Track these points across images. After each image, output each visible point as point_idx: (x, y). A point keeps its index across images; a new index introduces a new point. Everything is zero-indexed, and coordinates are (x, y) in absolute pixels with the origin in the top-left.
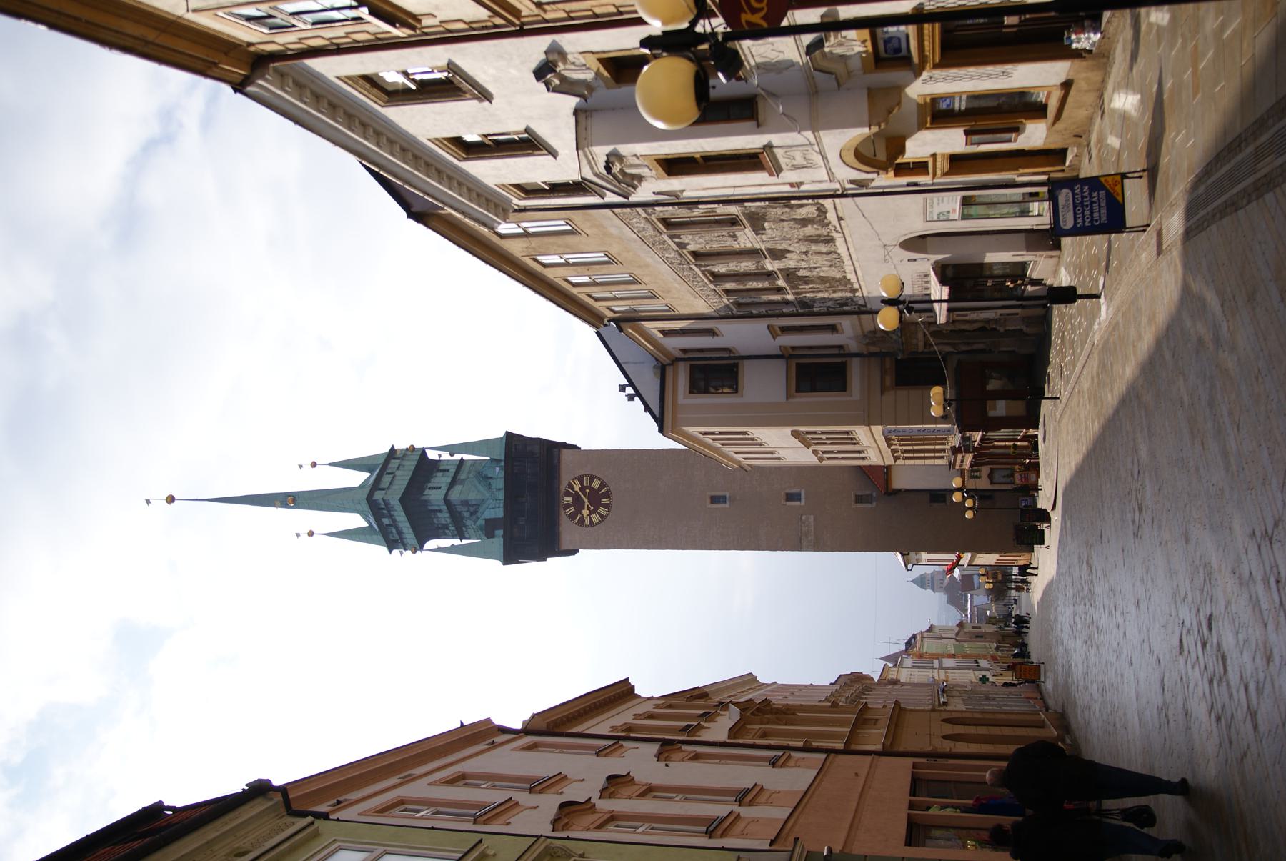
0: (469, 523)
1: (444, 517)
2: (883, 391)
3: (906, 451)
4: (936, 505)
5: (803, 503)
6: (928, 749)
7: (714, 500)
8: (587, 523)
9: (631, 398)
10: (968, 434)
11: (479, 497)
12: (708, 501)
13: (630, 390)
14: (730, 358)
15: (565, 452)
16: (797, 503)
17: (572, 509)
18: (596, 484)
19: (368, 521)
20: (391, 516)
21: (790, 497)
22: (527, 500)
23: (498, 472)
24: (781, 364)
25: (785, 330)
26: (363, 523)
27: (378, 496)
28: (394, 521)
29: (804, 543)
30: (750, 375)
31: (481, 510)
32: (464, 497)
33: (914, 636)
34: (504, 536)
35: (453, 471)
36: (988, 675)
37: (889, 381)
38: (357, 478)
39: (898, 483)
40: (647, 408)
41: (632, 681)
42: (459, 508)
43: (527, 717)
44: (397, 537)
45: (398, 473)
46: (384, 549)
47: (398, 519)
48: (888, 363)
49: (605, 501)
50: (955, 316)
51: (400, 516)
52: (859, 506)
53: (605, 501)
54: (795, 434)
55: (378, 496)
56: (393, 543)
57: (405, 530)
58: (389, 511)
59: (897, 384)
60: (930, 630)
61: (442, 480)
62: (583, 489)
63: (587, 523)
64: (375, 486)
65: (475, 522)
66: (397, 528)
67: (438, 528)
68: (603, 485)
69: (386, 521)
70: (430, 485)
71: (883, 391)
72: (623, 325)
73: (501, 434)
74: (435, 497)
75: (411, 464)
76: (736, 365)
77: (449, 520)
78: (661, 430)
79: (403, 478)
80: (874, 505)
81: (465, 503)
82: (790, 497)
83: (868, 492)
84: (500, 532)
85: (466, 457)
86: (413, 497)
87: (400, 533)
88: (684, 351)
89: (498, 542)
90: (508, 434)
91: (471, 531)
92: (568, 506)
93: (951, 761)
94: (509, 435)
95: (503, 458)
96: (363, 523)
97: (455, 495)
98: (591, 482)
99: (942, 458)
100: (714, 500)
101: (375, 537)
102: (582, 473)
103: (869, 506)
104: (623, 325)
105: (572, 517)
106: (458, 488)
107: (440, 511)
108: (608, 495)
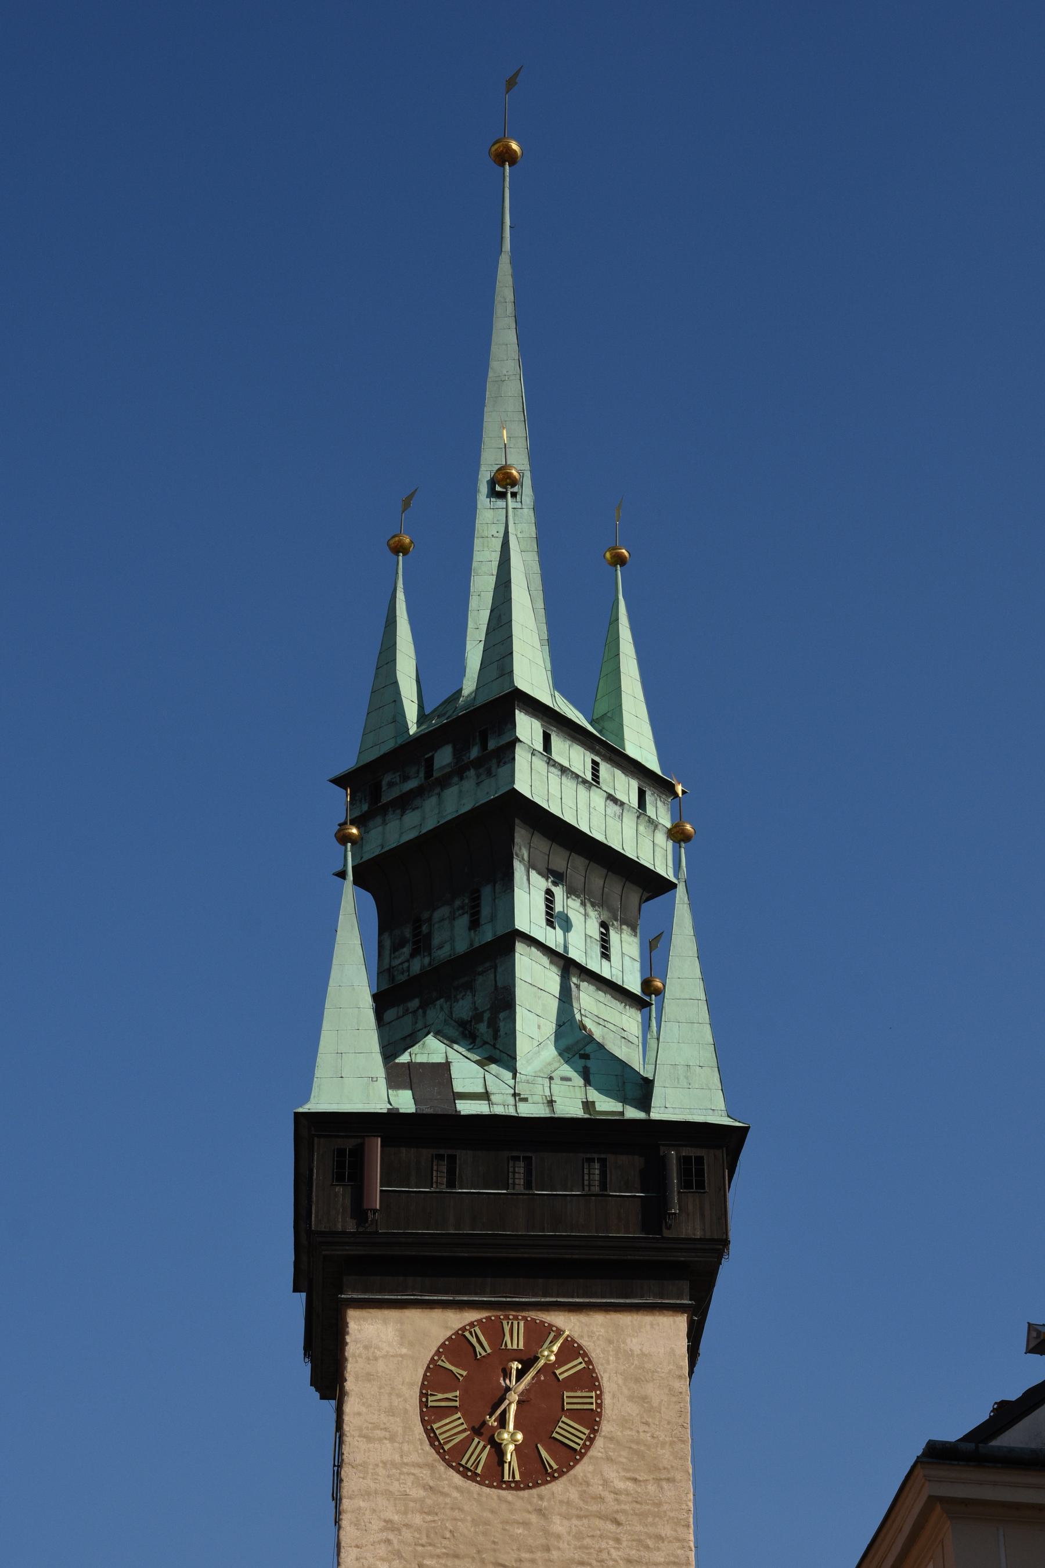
1: (452, 938)
8: (437, 1399)
20: (459, 770)
28: (444, 782)
44: (389, 795)
45: (597, 798)
46: (348, 762)
47: (451, 793)
57: (411, 818)
66: (420, 792)
77: (443, 954)
78: (936, 1454)
84: (405, 1101)
87: (404, 803)
95: (655, 1115)
98: (578, 1415)
107: (475, 924)
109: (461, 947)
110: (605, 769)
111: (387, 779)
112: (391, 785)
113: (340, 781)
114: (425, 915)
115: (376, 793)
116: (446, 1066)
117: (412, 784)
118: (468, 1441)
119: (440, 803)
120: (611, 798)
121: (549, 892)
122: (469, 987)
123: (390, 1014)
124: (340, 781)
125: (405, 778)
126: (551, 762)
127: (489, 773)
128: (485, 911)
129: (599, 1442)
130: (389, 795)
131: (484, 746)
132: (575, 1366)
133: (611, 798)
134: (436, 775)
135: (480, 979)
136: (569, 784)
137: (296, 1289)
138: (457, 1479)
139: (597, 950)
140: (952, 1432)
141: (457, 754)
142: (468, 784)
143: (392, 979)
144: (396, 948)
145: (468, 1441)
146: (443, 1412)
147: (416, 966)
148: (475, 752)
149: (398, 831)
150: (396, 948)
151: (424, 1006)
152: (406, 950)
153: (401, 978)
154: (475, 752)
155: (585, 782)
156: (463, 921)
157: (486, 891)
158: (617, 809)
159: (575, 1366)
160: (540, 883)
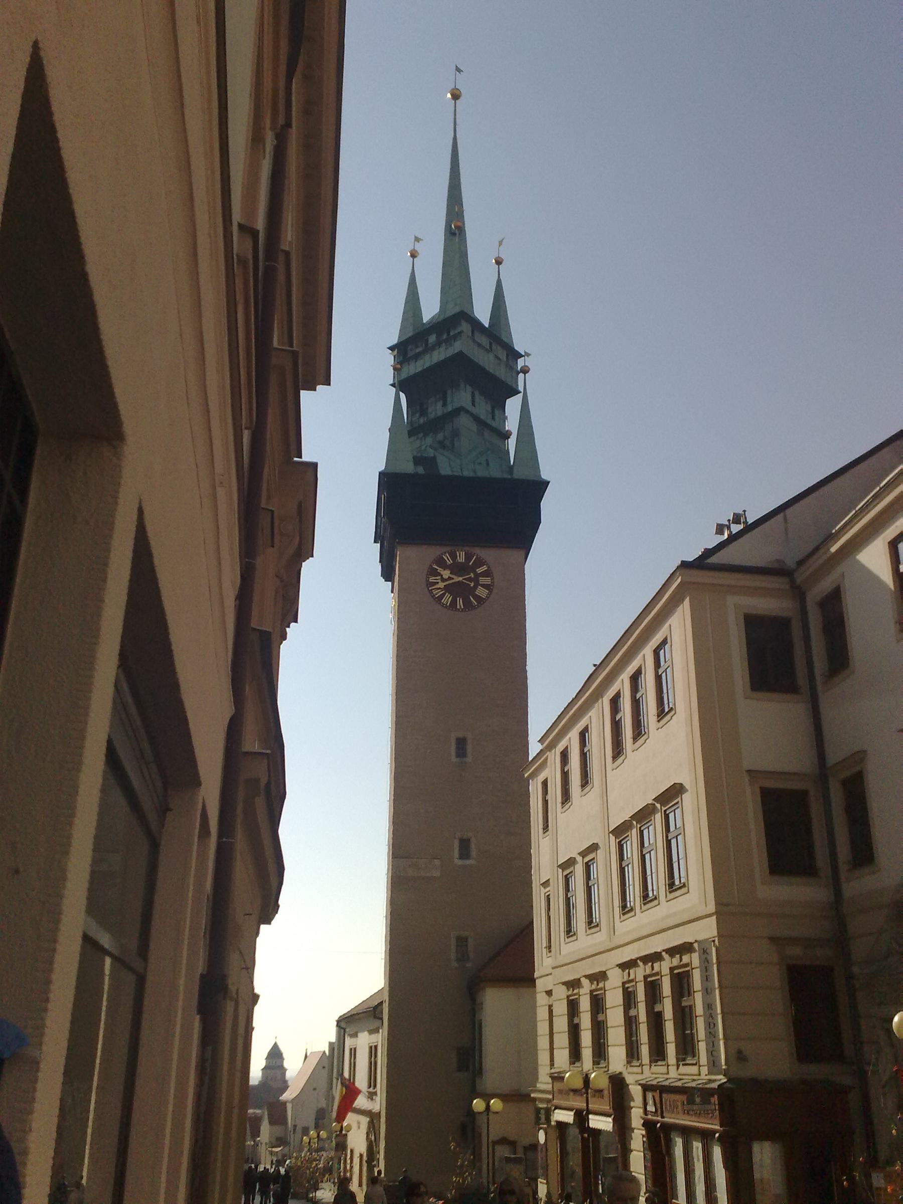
0: (429, 440)
1: (436, 409)
5: (459, 862)
7: (461, 743)
8: (432, 579)
10: (715, 1099)
16: (456, 853)
18: (481, 592)
20: (438, 344)
21: (465, 844)
23: (495, 472)
27: (465, 327)
28: (433, 348)
34: (415, 475)
35: (493, 424)
37: (795, 951)
38: (483, 313)
39: (495, 1002)
40: (708, 553)
44: (410, 354)
45: (491, 356)
46: (394, 341)
49: (460, 603)
50: (542, 1112)
51: (438, 356)
52: (453, 941)
55: (465, 327)
56: (402, 351)
61: (482, 409)
62: (477, 576)
63: (432, 579)
64: (476, 324)
65: (431, 447)
68: (479, 599)
69: (432, 339)
70: (477, 393)
73: (544, 476)
74: (463, 397)
75: (501, 373)
77: (432, 416)
78: (684, 565)
79: (486, 361)
80: (455, 964)
81: (456, 434)
82: (465, 844)
83: (471, 955)
84: (421, 470)
85: (512, 443)
86: (462, 370)
87: (417, 357)
89: (409, 467)
92: (453, 556)
94: (542, 486)
95: (515, 476)
97: (464, 421)
99: (575, 1054)
100: (461, 743)
103: (453, 956)
105: (441, 562)
106: (474, 427)
107: (445, 404)
108: (468, 605)
109: (439, 413)
110: (494, 347)
111: (410, 347)
112: (411, 350)
116: (434, 458)
117: (419, 350)
119: (431, 357)
120: (497, 357)
121: (473, 393)
124: (389, 348)
125: (417, 347)
126: (474, 341)
128: (449, 399)
130: (410, 354)
131: (449, 333)
132: (485, 568)
133: (497, 357)
134: (430, 345)
137: (375, 542)
139: (490, 416)
140: (690, 558)
142: (442, 349)
143: (412, 425)
147: (421, 421)
148: (445, 336)
149: (413, 369)
151: (425, 436)
152: (418, 415)
154: (445, 336)
155: (486, 350)
156: (440, 404)
157: (449, 392)
159: (485, 568)
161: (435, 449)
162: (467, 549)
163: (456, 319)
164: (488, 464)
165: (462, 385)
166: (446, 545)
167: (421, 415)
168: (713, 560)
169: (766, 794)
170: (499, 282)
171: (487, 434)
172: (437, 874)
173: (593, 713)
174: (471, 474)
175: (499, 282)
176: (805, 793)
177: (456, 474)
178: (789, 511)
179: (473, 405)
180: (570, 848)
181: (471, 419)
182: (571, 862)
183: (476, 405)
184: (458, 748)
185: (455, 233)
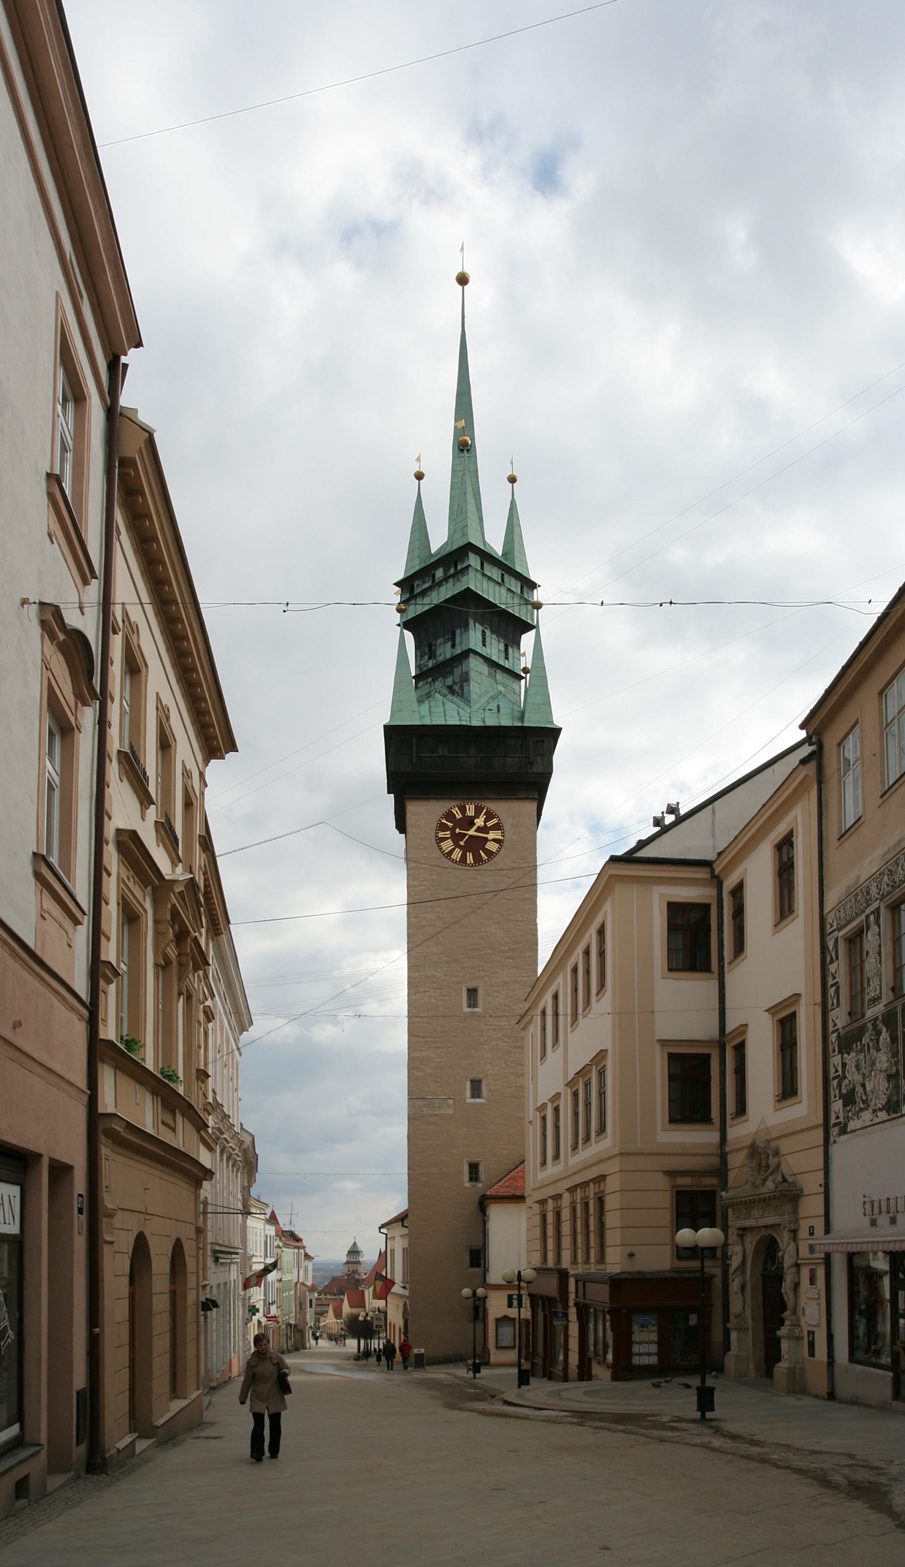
1: (445, 652)
2: (671, 1174)
3: (558, 1215)
4: (467, 1257)
6: (109, 1201)
7: (472, 993)
8: (441, 834)
9: (657, 822)
11: (473, 696)
12: (472, 985)
13: (669, 819)
14: (721, 958)
15: (534, 806)
16: (468, 1093)
17: (459, 816)
18: (492, 846)
19: (437, 552)
20: (446, 579)
22: (467, 770)
24: (715, 1032)
25: (787, 1026)
26: (435, 547)
27: (474, 560)
28: (440, 584)
29: (419, 1103)
30: (696, 990)
31: (455, 699)
32: (473, 675)
33: (298, 1240)
36: (259, 1316)
37: (684, 1182)
40: (641, 844)
41: (230, 755)
42: (457, 671)
43: (143, 418)
46: (400, 576)
47: (443, 589)
48: (709, 1182)
49: (470, 858)
52: (466, 1169)
53: (470, 858)
54: (601, 1055)
56: (406, 585)
57: (427, 600)
58: (453, 576)
59: (678, 1193)
60: (307, 1257)
61: (494, 649)
63: (441, 834)
64: (487, 557)
66: (430, 589)
67: (430, 646)
68: (490, 854)
70: (488, 632)
71: (671, 1174)
72: (813, 765)
73: (557, 722)
74: (474, 636)
76: (707, 969)
77: (441, 659)
78: (614, 859)
81: (465, 678)
87: (424, 593)
88: (738, 891)
90: (557, 732)
91: (427, 689)
92: (463, 810)
93: (80, 1243)
95: (525, 725)
96: (435, 547)
100: (472, 993)
101: (417, 561)
102: (506, 827)
104: (813, 765)
105: (449, 816)
106: (484, 668)
107: (453, 646)
108: (478, 860)
109: (448, 656)
110: (506, 577)
112: (418, 585)
113: (397, 584)
114: (433, 643)
115: (412, 590)
117: (426, 585)
118: (453, 850)
121: (483, 632)
122: (452, 672)
123: (420, 684)
124: (397, 584)
125: (424, 583)
126: (484, 575)
127: (458, 580)
128: (458, 640)
129: (502, 850)
134: (437, 581)
135: (456, 670)
136: (491, 584)
138: (450, 863)
139: (503, 655)
140: (620, 853)
141: (445, 571)
143: (421, 669)
144: (422, 657)
145: (453, 850)
146: (444, 839)
147: (430, 664)
148: (452, 571)
150: (422, 657)
151: (434, 681)
152: (426, 657)
153: (425, 669)
154: (452, 571)
155: (498, 583)
156: (449, 644)
157: (458, 632)
158: (511, 594)
160: (479, 627)
161: (445, 696)
162: (477, 802)
163: (456, 558)
164: (499, 711)
165: (471, 622)
166: (455, 799)
167: (430, 658)
168: (641, 854)
169: (673, 1058)
170: (513, 502)
171: (500, 676)
172: (451, 1112)
173: (560, 979)
174: (480, 724)
175: (513, 502)
176: (708, 1056)
177: (464, 723)
178: (716, 803)
179: (484, 645)
180: (544, 1097)
181: (482, 661)
182: (544, 1107)
183: (487, 644)
184: (469, 999)
185: (464, 447)
